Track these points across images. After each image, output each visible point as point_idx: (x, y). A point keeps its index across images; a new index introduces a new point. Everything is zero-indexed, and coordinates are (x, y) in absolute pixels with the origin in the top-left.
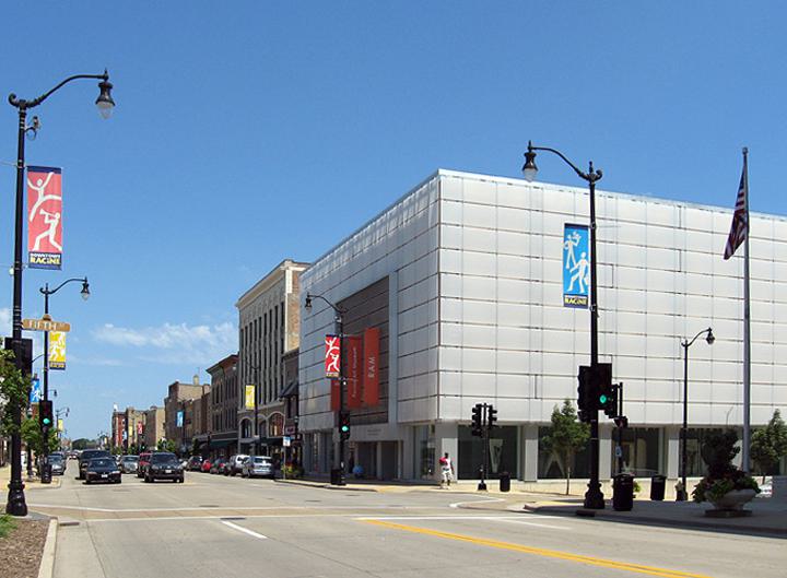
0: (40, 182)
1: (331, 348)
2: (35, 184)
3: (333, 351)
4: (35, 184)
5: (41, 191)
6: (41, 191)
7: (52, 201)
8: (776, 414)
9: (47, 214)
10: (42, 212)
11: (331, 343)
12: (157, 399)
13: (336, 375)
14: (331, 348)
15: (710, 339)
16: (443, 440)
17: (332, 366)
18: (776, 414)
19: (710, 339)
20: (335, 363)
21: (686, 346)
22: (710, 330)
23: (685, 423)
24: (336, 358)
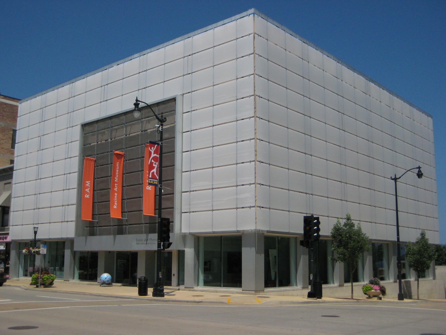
0: (152, 148)
1: (153, 155)
2: (151, 149)
3: (154, 158)
4: (151, 149)
5: (153, 152)
6: (153, 152)
7: (156, 156)
8: (423, 235)
9: (154, 162)
10: (153, 161)
11: (153, 150)
12: (368, 236)
13: (156, 182)
14: (153, 155)
15: (420, 175)
16: (148, 288)
17: (153, 173)
18: (423, 235)
19: (420, 175)
20: (155, 170)
21: (395, 179)
22: (419, 168)
23: (398, 239)
24: (156, 165)
